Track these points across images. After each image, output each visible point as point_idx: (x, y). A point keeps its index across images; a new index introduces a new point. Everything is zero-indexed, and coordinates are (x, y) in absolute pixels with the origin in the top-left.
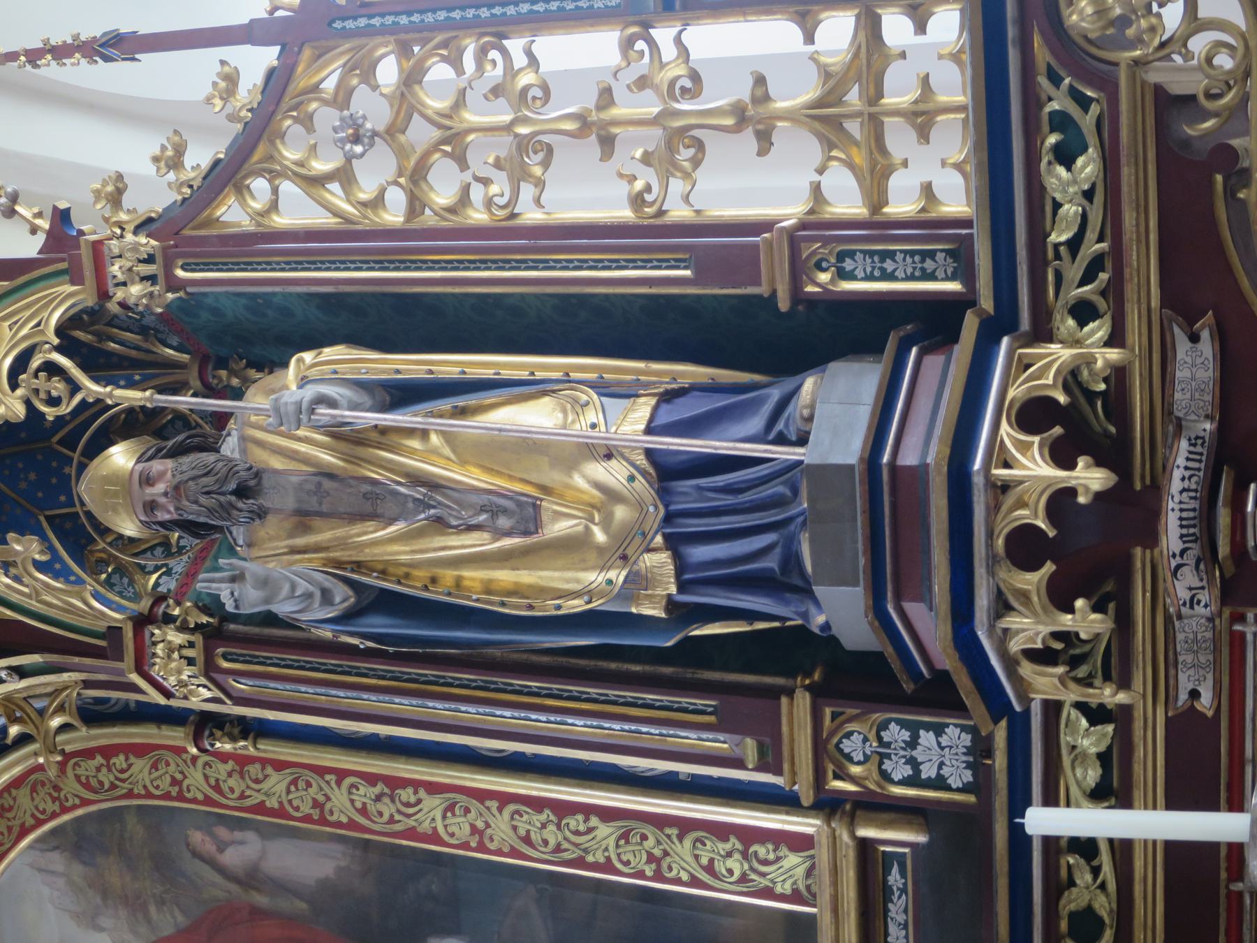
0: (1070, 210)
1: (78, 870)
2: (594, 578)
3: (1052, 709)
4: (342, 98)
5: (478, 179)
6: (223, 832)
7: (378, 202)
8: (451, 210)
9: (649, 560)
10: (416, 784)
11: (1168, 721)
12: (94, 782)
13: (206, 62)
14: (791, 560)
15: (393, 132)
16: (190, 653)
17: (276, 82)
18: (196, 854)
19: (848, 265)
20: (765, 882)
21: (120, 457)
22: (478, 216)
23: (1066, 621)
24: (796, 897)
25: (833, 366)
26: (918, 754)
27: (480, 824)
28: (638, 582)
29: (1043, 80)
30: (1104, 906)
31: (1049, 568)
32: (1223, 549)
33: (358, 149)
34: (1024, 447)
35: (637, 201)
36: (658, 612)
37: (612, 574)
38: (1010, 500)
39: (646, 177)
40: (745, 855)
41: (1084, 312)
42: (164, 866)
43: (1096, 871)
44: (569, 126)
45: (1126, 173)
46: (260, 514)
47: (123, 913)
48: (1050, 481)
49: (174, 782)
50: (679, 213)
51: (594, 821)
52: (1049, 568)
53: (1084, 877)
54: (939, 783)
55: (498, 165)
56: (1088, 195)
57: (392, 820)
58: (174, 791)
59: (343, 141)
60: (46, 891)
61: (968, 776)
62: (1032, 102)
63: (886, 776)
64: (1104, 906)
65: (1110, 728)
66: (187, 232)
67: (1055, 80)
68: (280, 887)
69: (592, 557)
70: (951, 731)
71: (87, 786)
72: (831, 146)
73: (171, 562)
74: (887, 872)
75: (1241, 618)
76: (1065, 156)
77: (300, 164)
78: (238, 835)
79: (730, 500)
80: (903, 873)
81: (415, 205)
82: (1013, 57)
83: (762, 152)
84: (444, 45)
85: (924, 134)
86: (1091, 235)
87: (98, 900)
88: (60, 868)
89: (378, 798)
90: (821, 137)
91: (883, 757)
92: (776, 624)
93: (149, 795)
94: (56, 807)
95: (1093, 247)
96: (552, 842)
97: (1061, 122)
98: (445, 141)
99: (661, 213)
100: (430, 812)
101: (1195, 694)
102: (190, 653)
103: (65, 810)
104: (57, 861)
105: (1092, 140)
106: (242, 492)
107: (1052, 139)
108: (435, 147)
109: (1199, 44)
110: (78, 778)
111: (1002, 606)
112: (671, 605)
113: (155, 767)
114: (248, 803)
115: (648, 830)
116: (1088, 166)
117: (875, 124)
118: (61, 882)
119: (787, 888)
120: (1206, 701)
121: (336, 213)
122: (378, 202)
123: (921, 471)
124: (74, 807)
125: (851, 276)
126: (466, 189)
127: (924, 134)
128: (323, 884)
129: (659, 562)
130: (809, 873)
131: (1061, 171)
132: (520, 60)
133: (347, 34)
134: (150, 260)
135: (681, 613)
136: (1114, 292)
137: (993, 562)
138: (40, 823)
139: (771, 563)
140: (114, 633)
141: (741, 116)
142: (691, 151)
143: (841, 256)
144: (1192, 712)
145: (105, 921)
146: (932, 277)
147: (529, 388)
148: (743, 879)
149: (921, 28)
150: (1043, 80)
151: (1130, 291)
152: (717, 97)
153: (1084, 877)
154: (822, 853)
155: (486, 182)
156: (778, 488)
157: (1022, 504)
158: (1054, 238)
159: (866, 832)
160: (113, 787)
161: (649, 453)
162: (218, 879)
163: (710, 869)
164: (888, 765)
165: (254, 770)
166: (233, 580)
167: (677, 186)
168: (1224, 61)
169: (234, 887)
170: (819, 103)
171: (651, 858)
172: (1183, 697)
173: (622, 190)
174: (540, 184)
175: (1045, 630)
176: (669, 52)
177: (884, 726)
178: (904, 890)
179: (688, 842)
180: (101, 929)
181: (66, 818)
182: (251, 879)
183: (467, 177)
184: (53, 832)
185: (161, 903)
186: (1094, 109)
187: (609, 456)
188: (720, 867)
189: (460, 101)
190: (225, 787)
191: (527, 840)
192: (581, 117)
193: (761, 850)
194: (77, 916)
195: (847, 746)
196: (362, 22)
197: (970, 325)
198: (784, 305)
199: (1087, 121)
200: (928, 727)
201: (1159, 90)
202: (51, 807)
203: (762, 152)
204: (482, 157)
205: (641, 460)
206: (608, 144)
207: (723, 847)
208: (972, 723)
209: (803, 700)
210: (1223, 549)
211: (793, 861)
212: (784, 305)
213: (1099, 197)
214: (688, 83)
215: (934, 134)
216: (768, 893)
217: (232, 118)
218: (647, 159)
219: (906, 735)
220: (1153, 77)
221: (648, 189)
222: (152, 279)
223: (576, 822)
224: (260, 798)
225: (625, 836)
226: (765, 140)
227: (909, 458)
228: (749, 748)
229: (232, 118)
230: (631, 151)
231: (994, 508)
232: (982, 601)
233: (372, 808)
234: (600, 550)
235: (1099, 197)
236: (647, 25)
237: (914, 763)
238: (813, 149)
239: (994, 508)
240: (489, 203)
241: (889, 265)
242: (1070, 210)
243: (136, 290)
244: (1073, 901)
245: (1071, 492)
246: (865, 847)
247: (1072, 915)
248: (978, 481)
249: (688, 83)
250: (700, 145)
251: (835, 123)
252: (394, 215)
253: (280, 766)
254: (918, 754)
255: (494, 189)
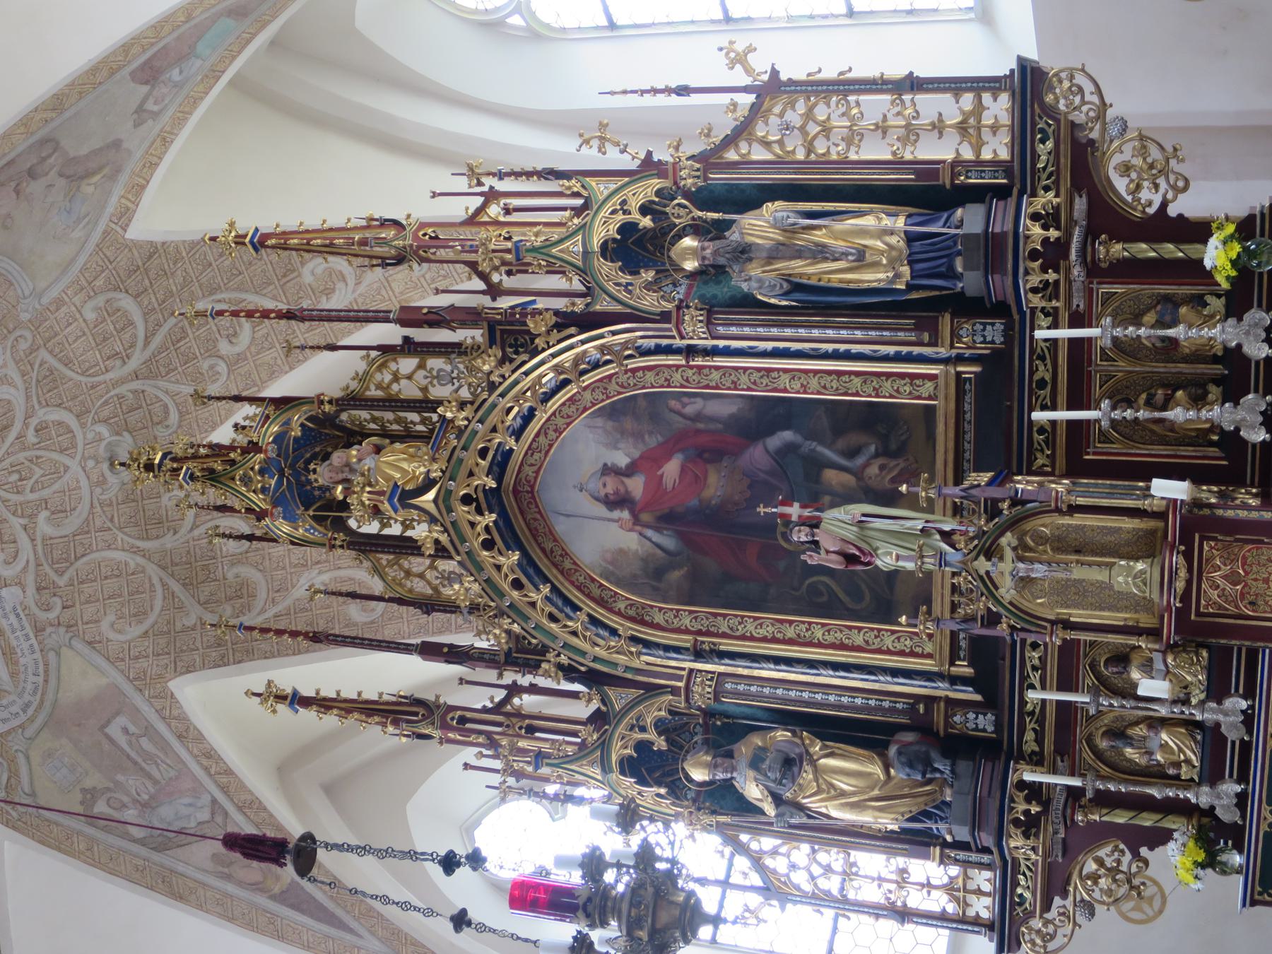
0: (1044, 158)
1: (610, 424)
2: (881, 276)
3: (1033, 310)
4: (781, 115)
5: (834, 144)
6: (685, 400)
7: (793, 152)
8: (824, 155)
9: (902, 269)
10: (778, 370)
11: (1069, 315)
12: (625, 384)
13: (725, 98)
14: (951, 267)
15: (802, 129)
16: (701, 318)
17: (755, 109)
18: (672, 410)
19: (970, 174)
20: (918, 394)
21: (688, 242)
22: (834, 157)
23: (1046, 276)
24: (930, 398)
25: (968, 205)
26: (986, 333)
27: (805, 383)
28: (897, 276)
29: (1037, 118)
30: (1048, 377)
31: (1040, 261)
32: (1089, 259)
33: (788, 132)
34: (1034, 226)
35: (894, 153)
36: (904, 287)
37: (889, 274)
38: (1030, 240)
39: (897, 145)
40: (911, 384)
41: (1047, 189)
42: (655, 418)
43: (1045, 365)
44: (872, 127)
45: (1062, 147)
46: (750, 260)
47: (631, 440)
48: (1042, 235)
49: (666, 380)
50: (908, 157)
51: (853, 377)
52: (1040, 261)
53: (1041, 368)
54: (993, 342)
55: (843, 139)
56: (1049, 153)
57: (767, 385)
58: (666, 384)
59: (782, 130)
60: (591, 436)
61: (1002, 339)
62: (1034, 124)
63: (974, 342)
64: (1048, 377)
65: (1051, 318)
66: (712, 161)
67: (1041, 118)
68: (711, 419)
69: (882, 269)
70: (998, 325)
71: (622, 386)
72: (964, 136)
73: (678, 289)
74: (965, 384)
75: (1092, 283)
76: (1043, 141)
77: (763, 137)
78: (692, 400)
79: (931, 248)
80: (970, 385)
81: (809, 152)
82: (1029, 110)
83: (939, 138)
84: (825, 98)
85: (994, 134)
86: (1050, 165)
87: (619, 436)
88: (600, 424)
89: (762, 377)
90: (960, 133)
91: (974, 335)
92: (937, 293)
93: (653, 387)
94: (604, 397)
95: (1050, 169)
96: (835, 387)
97: (1042, 131)
98: (823, 131)
99: (902, 157)
100: (785, 380)
101: (1078, 306)
102: (701, 318)
103: (608, 398)
104: (599, 422)
105: (1051, 136)
106: (743, 252)
107: (1039, 136)
108: (819, 133)
109: (1085, 108)
110: (617, 383)
111: (1027, 273)
112: (908, 284)
113: (657, 374)
114: (701, 385)
115: (874, 378)
116: (1050, 144)
117: (979, 129)
118: (600, 431)
119: (927, 395)
120: (1082, 306)
121: (775, 154)
122: (793, 152)
123: (1004, 234)
124: (614, 396)
125: (970, 178)
126: (829, 148)
127: (994, 134)
128: (732, 416)
129: (906, 270)
130: (935, 388)
131: (1041, 146)
132: (853, 104)
133: (786, 92)
134: (698, 170)
135: (910, 288)
136: (1057, 183)
137: (1025, 259)
138: (594, 405)
139: (943, 269)
140: (669, 313)
141: (934, 126)
142: (915, 137)
143: (967, 172)
144: (1077, 311)
145: (621, 445)
146: (997, 178)
147: (861, 214)
148: (910, 393)
149: (995, 100)
150: (1037, 118)
151: (1062, 182)
152: (924, 121)
153: (1041, 368)
154: (941, 381)
155: (837, 145)
156: (950, 243)
157: (1033, 242)
158: (1038, 166)
159: (960, 369)
160: (635, 385)
161: (906, 232)
162: (681, 419)
163: (898, 391)
164: (975, 338)
165: (706, 371)
166: (746, 280)
167: (909, 148)
168: (1092, 114)
169: (688, 422)
170: (961, 123)
171: (875, 389)
172: (1075, 306)
173: (890, 149)
174: (859, 147)
175: (1039, 279)
176: (908, 104)
177: (974, 325)
178: (970, 391)
179: (889, 382)
180: (619, 449)
181: (608, 401)
182: (698, 417)
183: (830, 143)
184: (599, 409)
185: (651, 433)
186: (1052, 127)
187: (892, 234)
188: (901, 390)
189: (829, 118)
190: (691, 380)
191: (824, 387)
192: (876, 125)
193: (917, 382)
194: (607, 445)
195: (961, 332)
196: (793, 88)
197: (1015, 191)
198: (948, 186)
199: (1050, 131)
200: (989, 324)
201: (1072, 122)
202: (601, 397)
203: (939, 138)
204: (836, 136)
205: (903, 235)
206: (885, 133)
207: (903, 382)
208: (579, 740)
209: (948, 317)
210: (1089, 259)
211: (929, 385)
212: (948, 186)
213: (1053, 154)
214: (915, 114)
215: (998, 133)
216: (919, 398)
217: (735, 119)
218: (898, 139)
219: (982, 327)
220: (1070, 117)
221: (898, 149)
222: (698, 177)
223: (845, 378)
224: (707, 382)
225: (865, 382)
226: (941, 134)
227: (997, 230)
228: (926, 337)
229: (735, 119)
230: (893, 136)
231: (1025, 243)
232: (1021, 271)
233: (758, 381)
234: (885, 266)
235: (1053, 154)
236: (901, 95)
237: (984, 336)
238: (957, 138)
239: (1025, 243)
240: (838, 153)
241: (983, 175)
242: (1044, 158)
243: (690, 181)
244: (1036, 377)
245: (1049, 238)
246: (958, 374)
247: (1037, 381)
248: (1021, 234)
249: (915, 114)
250: (918, 135)
251: (965, 129)
252: (800, 155)
253: (717, 368)
254: (986, 333)
255: (840, 148)
